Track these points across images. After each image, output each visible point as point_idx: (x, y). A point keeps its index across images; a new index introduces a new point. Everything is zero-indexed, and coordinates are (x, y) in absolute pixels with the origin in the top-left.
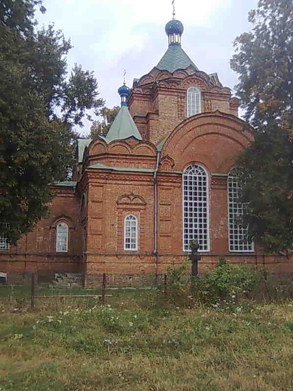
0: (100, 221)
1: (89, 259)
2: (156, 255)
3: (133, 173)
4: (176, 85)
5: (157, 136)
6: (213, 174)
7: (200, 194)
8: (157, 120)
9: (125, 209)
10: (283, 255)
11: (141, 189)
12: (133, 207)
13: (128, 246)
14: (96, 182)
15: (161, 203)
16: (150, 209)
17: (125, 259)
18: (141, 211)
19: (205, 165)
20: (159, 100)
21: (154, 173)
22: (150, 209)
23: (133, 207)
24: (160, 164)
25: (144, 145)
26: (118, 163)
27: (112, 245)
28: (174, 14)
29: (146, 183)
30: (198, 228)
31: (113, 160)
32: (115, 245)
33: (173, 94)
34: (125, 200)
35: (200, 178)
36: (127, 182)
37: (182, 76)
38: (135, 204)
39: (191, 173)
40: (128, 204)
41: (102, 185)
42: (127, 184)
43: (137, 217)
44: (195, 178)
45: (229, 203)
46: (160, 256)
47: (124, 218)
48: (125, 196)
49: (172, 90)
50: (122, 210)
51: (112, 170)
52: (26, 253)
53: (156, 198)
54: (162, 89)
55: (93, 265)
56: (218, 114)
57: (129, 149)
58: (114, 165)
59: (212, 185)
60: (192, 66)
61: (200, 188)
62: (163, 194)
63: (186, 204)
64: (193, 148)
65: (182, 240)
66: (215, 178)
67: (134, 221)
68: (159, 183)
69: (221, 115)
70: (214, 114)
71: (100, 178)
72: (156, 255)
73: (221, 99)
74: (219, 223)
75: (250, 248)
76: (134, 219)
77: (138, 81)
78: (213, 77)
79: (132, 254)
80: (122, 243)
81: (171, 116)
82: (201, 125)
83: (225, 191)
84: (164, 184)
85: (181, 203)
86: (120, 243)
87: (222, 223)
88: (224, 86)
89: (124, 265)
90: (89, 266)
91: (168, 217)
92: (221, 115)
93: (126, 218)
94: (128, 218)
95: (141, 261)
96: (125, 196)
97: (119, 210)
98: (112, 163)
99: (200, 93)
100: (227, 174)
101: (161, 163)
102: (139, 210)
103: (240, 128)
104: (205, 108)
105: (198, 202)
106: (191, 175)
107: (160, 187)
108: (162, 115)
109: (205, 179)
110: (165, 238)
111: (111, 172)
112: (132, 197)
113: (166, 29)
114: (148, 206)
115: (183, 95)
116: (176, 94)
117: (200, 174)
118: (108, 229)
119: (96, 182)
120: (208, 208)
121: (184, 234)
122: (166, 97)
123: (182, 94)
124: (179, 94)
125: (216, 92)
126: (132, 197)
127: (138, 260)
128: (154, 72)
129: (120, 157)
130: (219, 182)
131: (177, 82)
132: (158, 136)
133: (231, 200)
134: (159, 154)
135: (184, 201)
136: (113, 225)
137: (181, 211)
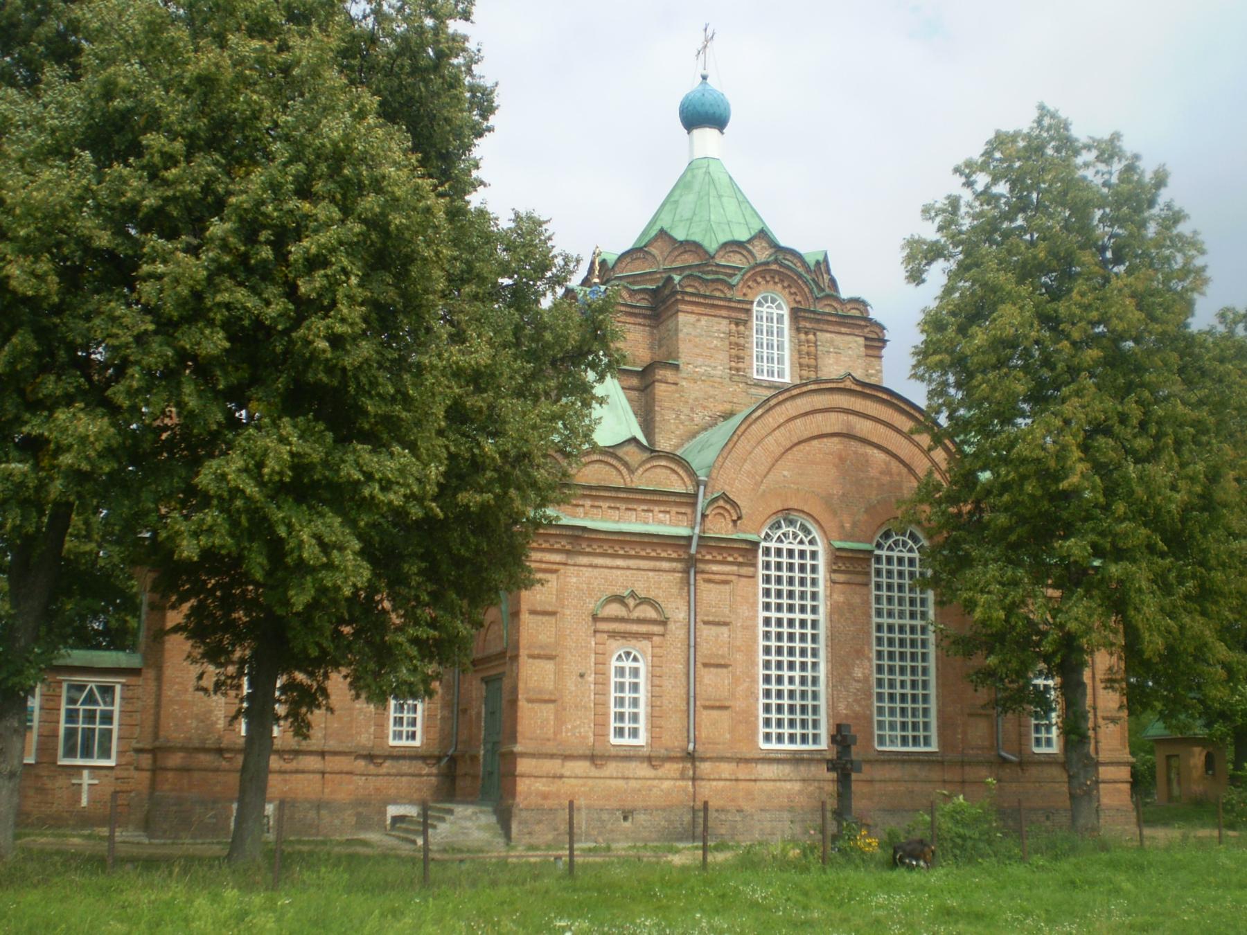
0: (549, 666)
1: (523, 766)
2: (691, 757)
3: (615, 537)
4: (726, 291)
5: (673, 427)
6: (838, 544)
7: (803, 596)
8: (676, 384)
9: (613, 635)
10: (1011, 762)
11: (657, 581)
12: (634, 628)
13: (620, 732)
14: (541, 562)
15: (706, 619)
16: (677, 632)
17: (612, 768)
18: (655, 638)
19: (817, 521)
20: (680, 326)
21: (690, 538)
22: (677, 632)
23: (634, 628)
24: (704, 516)
25: (663, 463)
26: (595, 511)
27: (579, 731)
28: (704, 78)
29: (665, 565)
30: (908, 691)
31: (601, 504)
32: (588, 731)
33: (718, 312)
34: (615, 609)
35: (802, 554)
36: (620, 562)
37: (736, 260)
38: (640, 621)
39: (779, 540)
40: (626, 619)
41: (555, 567)
42: (618, 568)
43: (644, 656)
44: (791, 553)
45: (875, 620)
46: (703, 760)
47: (611, 657)
48: (619, 599)
49: (716, 302)
50: (605, 636)
51: (584, 529)
52: (326, 748)
53: (693, 606)
54: (687, 298)
55: (533, 782)
56: (849, 384)
57: (625, 471)
58: (586, 514)
59: (835, 571)
60: (763, 234)
61: (802, 582)
62: (710, 595)
63: (767, 621)
64: (785, 471)
65: (757, 717)
66: (843, 554)
67: (635, 665)
68: (701, 566)
69: (858, 388)
70: (841, 385)
71: (552, 550)
72: (691, 757)
73: (843, 330)
74: (849, 673)
75: (927, 743)
76: (635, 659)
77: (610, 264)
78: (818, 263)
79: (628, 756)
80: (605, 725)
81: (713, 372)
82: (806, 414)
83: (864, 590)
84: (715, 568)
85: (755, 617)
86: (601, 725)
87: (858, 673)
88: (845, 293)
89: (612, 782)
90: (522, 786)
91: (723, 657)
92: (858, 388)
93: (615, 656)
94: (620, 656)
95: (652, 773)
96: (619, 599)
97: (598, 635)
98: (581, 509)
99: (786, 312)
100: (871, 543)
101: (708, 512)
102: (648, 636)
103: (906, 424)
104: (799, 352)
105: (797, 616)
106: (779, 545)
107: (706, 576)
108: (687, 369)
109: (814, 555)
110: (715, 713)
111: (580, 533)
112: (631, 602)
113: (681, 112)
114: (671, 626)
115: (743, 316)
116: (724, 313)
117: (801, 542)
118: (571, 683)
119: (541, 562)
120: (822, 632)
121: (613, 695)
122: (699, 320)
123: (740, 315)
124: (734, 315)
125: (827, 310)
126: (631, 602)
127: (643, 770)
128: (659, 243)
129: (602, 494)
130: (851, 564)
131: (722, 278)
132: (677, 427)
133: (879, 613)
134: (702, 488)
135: (762, 614)
136: (582, 676)
137: (755, 641)
